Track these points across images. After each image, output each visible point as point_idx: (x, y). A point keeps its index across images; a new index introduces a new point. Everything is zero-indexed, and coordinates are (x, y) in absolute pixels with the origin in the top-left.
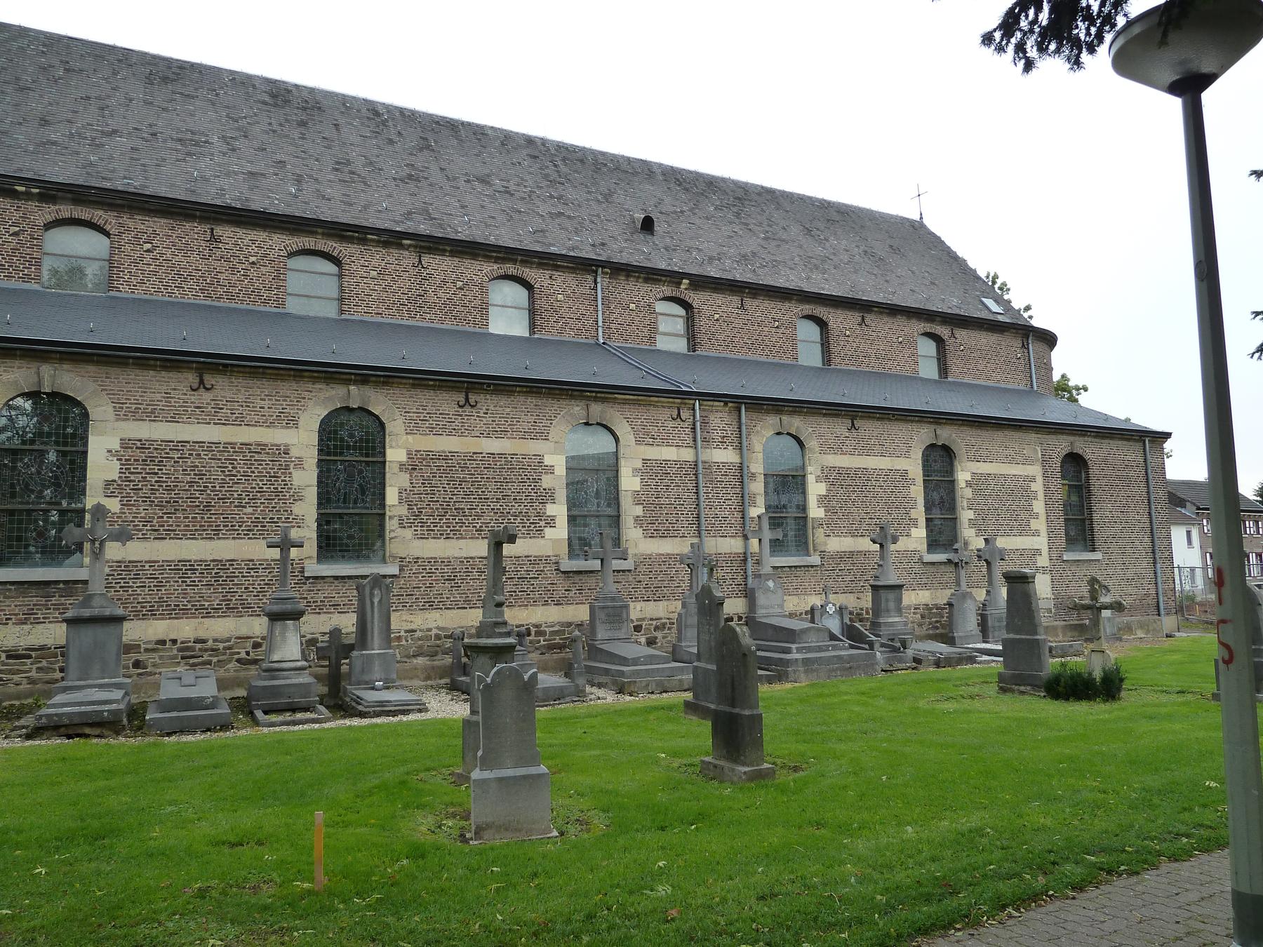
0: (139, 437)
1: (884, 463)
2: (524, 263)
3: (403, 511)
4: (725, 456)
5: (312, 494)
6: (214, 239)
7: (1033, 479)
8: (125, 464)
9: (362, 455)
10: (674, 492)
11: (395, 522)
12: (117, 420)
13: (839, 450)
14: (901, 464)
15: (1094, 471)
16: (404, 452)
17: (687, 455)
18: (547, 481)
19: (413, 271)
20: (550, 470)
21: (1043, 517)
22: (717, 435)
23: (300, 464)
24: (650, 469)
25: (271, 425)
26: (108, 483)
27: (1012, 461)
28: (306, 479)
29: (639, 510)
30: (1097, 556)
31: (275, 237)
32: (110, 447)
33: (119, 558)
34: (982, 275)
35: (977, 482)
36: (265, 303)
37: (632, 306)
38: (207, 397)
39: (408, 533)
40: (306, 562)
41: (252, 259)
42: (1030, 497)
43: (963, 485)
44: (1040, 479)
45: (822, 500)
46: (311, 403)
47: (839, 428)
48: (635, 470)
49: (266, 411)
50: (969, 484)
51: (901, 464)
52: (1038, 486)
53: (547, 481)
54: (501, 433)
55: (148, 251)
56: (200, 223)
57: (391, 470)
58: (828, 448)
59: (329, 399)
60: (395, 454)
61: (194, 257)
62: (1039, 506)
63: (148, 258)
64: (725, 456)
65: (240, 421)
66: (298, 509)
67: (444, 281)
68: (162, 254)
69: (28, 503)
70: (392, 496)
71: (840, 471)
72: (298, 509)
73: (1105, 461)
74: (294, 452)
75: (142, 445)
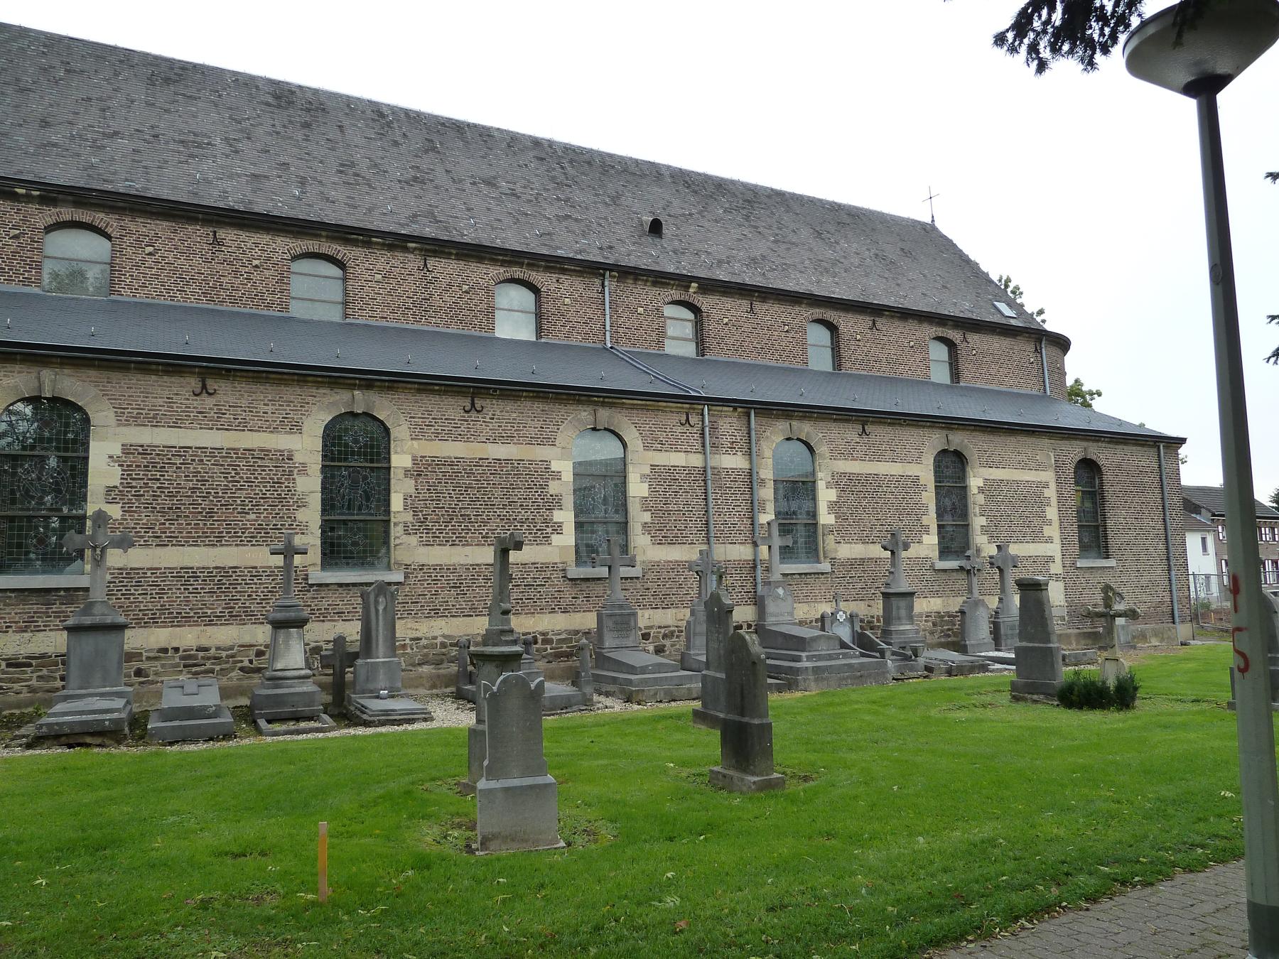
0: (141, 442)
1: (895, 469)
2: (531, 266)
3: (409, 517)
4: (734, 461)
5: (315, 501)
6: (217, 242)
7: (1046, 486)
8: (127, 470)
9: (366, 461)
10: (682, 498)
11: (400, 528)
12: (119, 425)
13: (849, 455)
14: (912, 470)
15: (1108, 477)
16: (409, 458)
17: (696, 460)
18: (554, 487)
19: (418, 275)
20: (557, 476)
21: (1056, 524)
22: (726, 441)
23: (303, 470)
24: (658, 475)
25: (275, 430)
26: (110, 489)
27: (1024, 467)
28: (310, 485)
29: (647, 517)
30: (1111, 563)
31: (279, 240)
32: (111, 453)
33: (121, 566)
34: (995, 278)
35: (989, 488)
36: (268, 307)
37: (640, 310)
38: (209, 402)
39: (413, 540)
40: (310, 569)
41: (256, 262)
42: (1043, 503)
43: (976, 491)
44: (1053, 486)
45: (833, 506)
46: (315, 408)
47: (850, 433)
48: (643, 476)
49: (269, 417)
50: (981, 490)
51: (912, 470)
52: (1051, 492)
53: (554, 487)
54: (507, 439)
55: (150, 254)
56: (202, 226)
57: (396, 476)
58: (838, 454)
59: (333, 404)
60: (400, 460)
61: (197, 260)
62: (1052, 513)
63: (150, 261)
64: (734, 461)
65: (243, 427)
66: (301, 515)
67: (449, 285)
68: (164, 258)
69: (28, 509)
70: (397, 502)
71: (850, 477)
72: (301, 515)
73: (1119, 466)
74: (298, 458)
75: (144, 450)
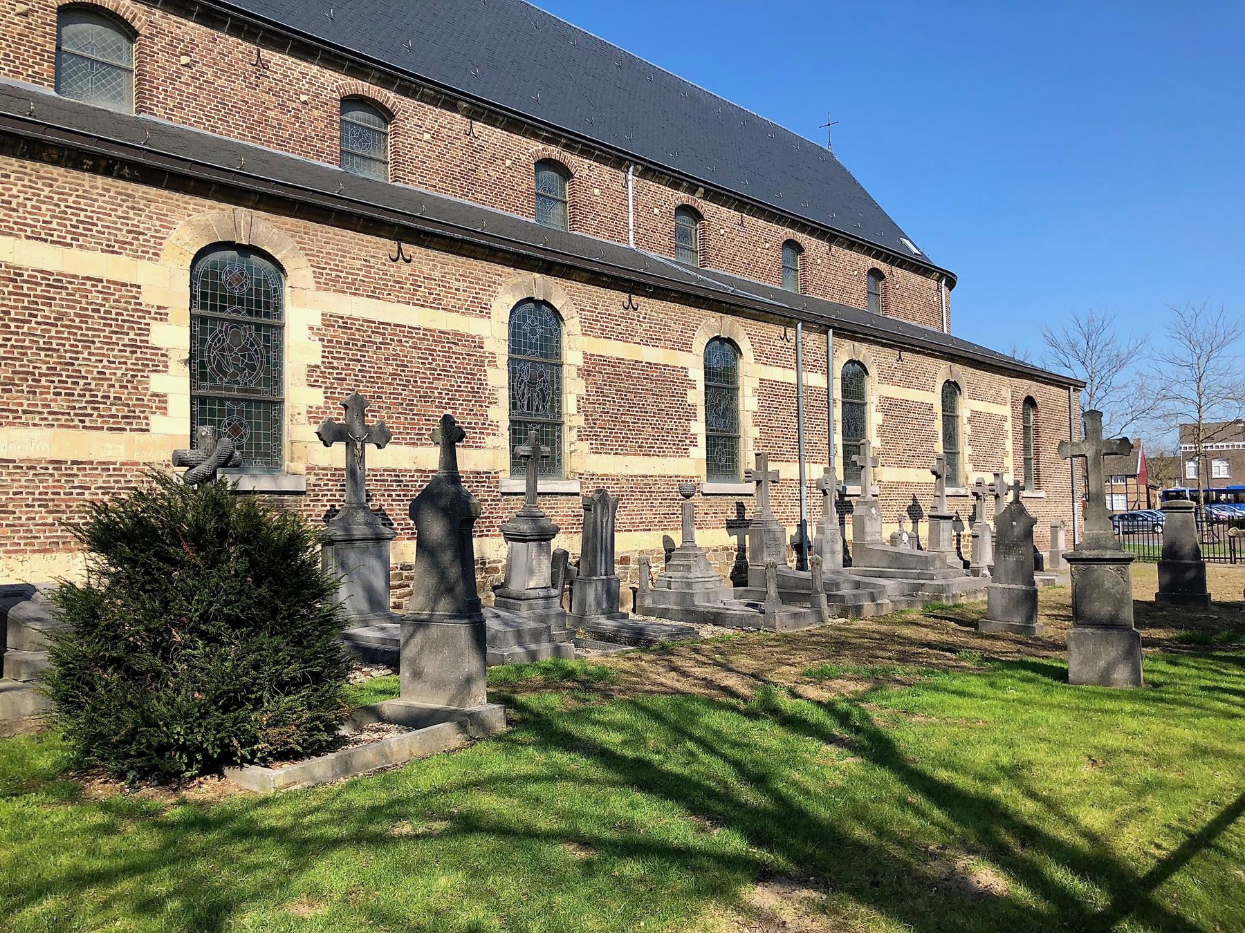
0: (341, 313)
2: (568, 147)
3: (580, 421)
5: (504, 396)
8: (328, 344)
9: (250, 312)
11: (574, 432)
12: (318, 289)
16: (581, 355)
17: (790, 376)
19: (465, 140)
23: (161, 314)
24: (767, 389)
25: (466, 312)
26: (313, 369)
30: (1042, 494)
31: (328, 73)
32: (312, 324)
33: (325, 465)
36: (318, 155)
37: (656, 211)
38: (406, 269)
39: (585, 446)
40: (501, 475)
41: (303, 98)
43: (965, 421)
46: (500, 289)
48: (755, 390)
49: (461, 295)
52: (1008, 426)
55: (185, 66)
56: (245, 39)
59: (516, 286)
61: (239, 84)
62: (1009, 445)
63: (187, 73)
67: (494, 157)
68: (202, 74)
69: (220, 388)
70: (570, 404)
74: (488, 347)
75: (345, 323)
